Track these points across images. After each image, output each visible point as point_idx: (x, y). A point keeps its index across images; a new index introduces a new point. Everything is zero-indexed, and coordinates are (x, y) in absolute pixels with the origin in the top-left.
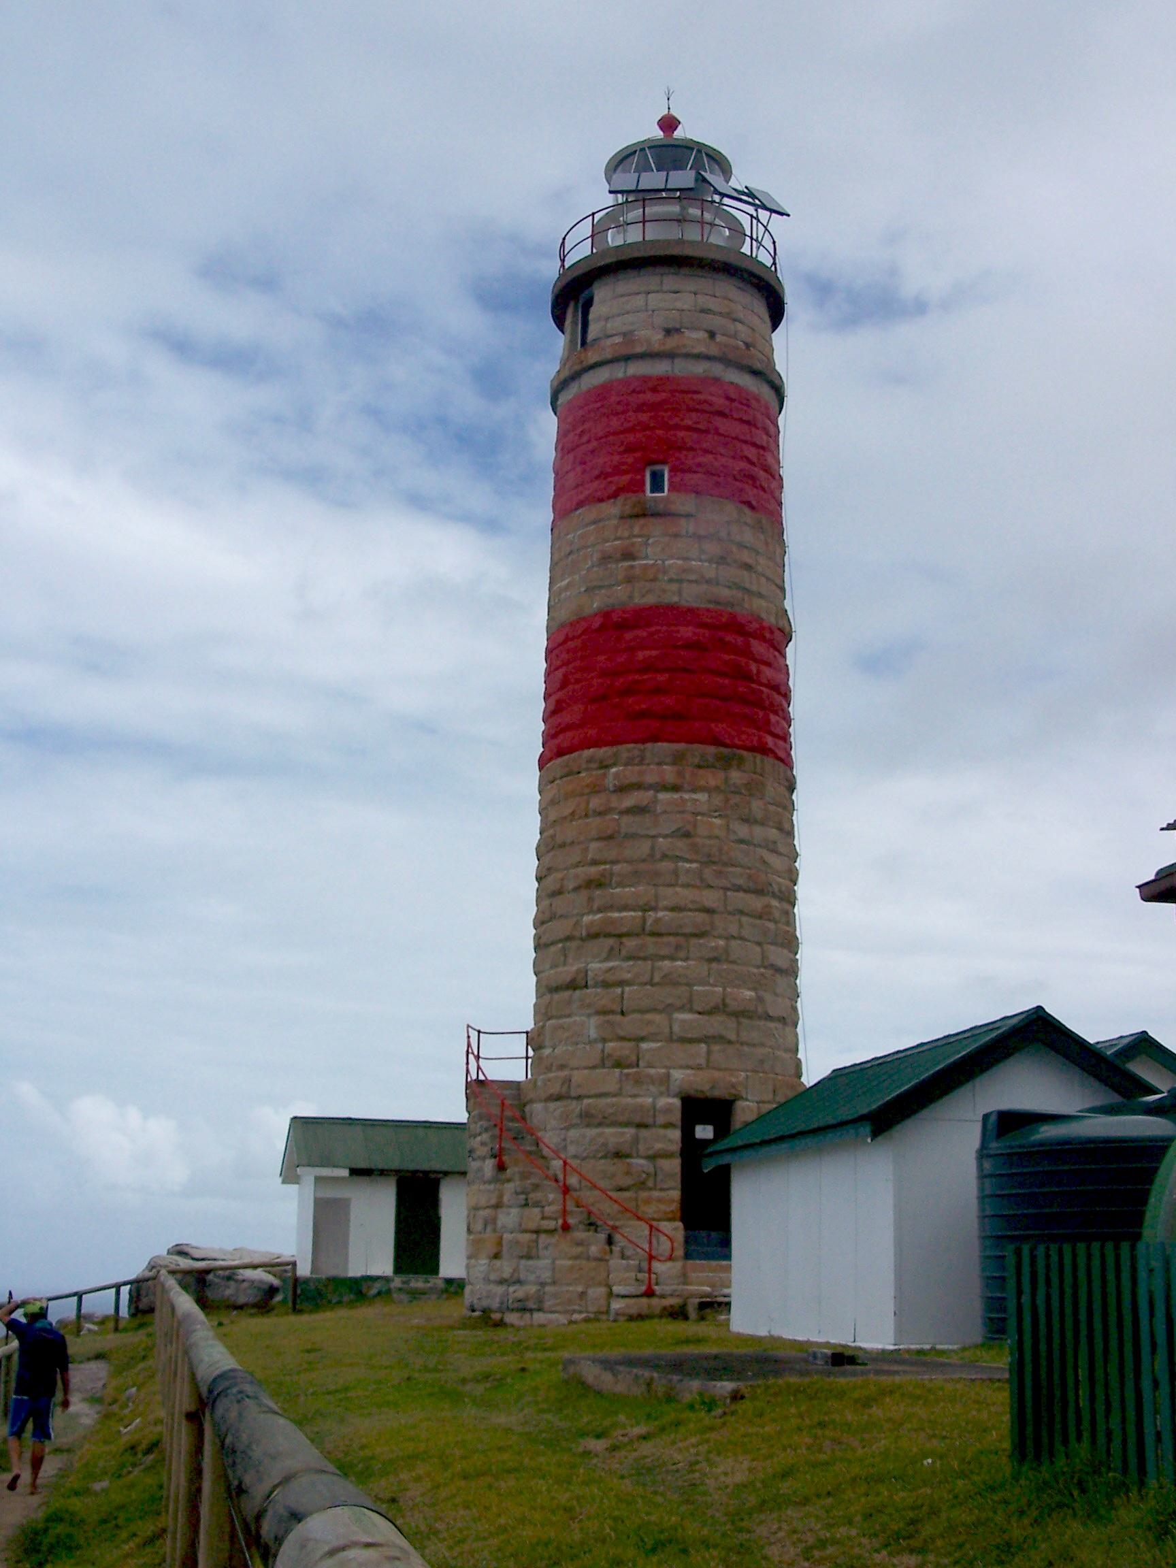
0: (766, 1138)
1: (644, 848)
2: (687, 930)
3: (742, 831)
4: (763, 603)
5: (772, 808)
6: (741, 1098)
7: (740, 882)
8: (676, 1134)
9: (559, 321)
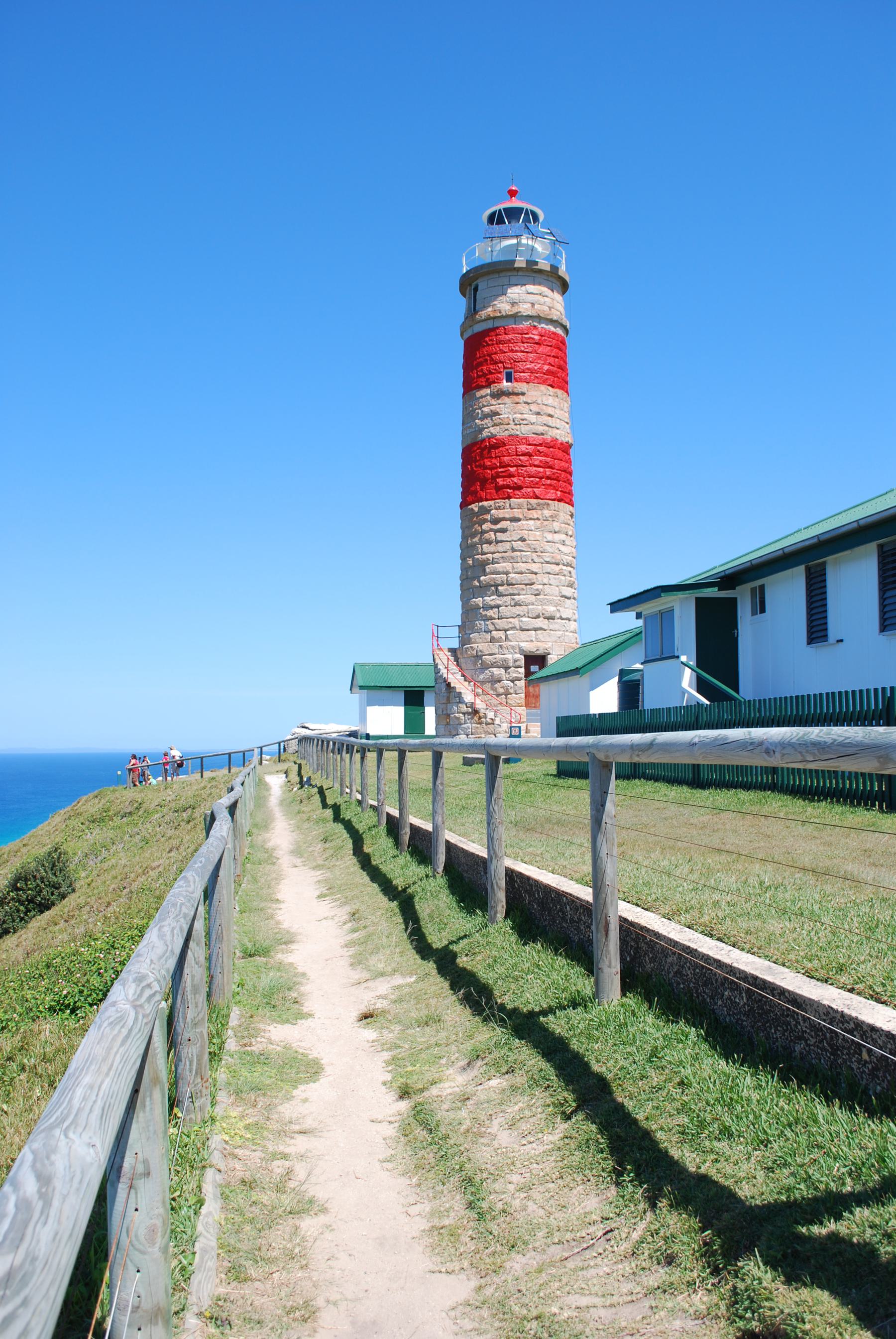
0: (178, 951)
1: (507, 546)
2: (526, 582)
3: (550, 537)
4: (558, 431)
5: (563, 525)
6: (549, 654)
7: (548, 560)
8: (522, 670)
9: (463, 293)
